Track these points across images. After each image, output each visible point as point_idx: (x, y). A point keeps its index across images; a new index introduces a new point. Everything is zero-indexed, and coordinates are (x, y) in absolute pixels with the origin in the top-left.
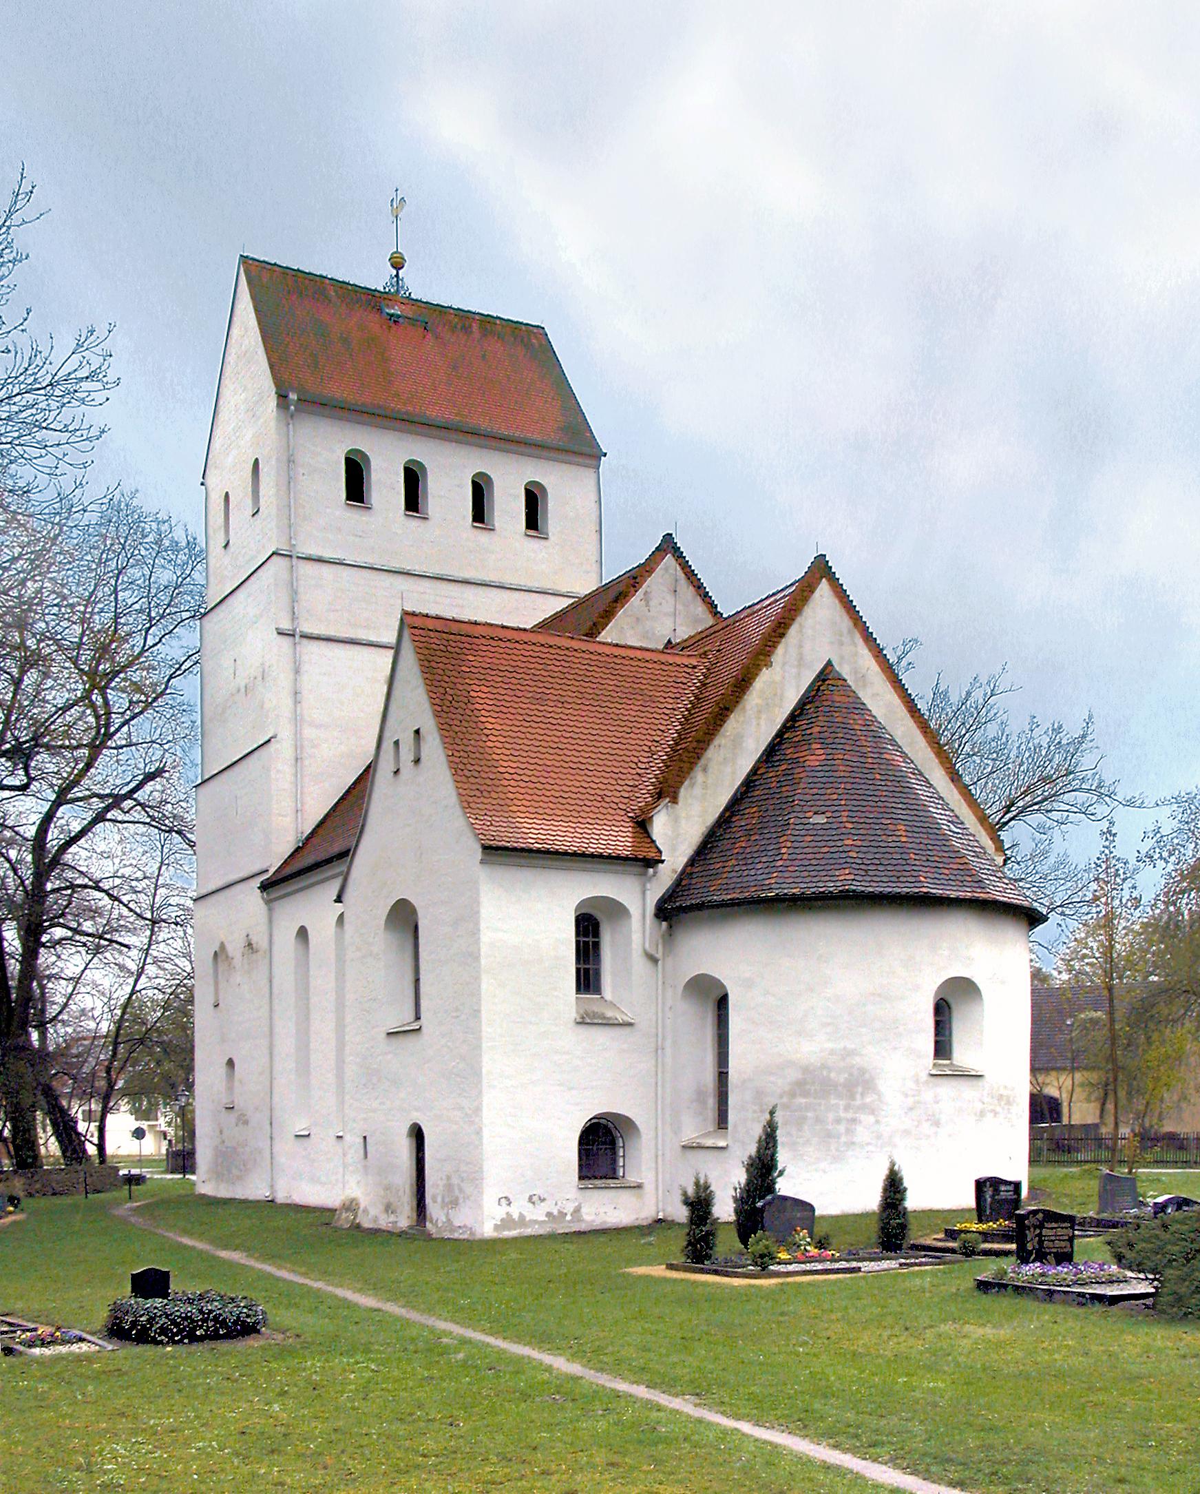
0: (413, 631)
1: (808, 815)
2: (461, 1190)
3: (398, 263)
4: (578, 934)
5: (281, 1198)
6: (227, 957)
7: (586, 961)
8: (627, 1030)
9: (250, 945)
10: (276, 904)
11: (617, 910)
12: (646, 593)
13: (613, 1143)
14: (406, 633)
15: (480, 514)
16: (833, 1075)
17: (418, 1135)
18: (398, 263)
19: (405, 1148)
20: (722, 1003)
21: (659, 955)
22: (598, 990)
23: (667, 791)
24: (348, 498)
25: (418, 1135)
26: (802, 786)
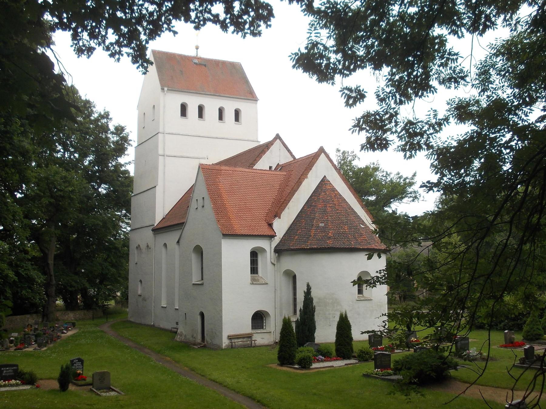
0: (203, 170)
1: (319, 223)
2: (216, 333)
3: (197, 48)
4: (251, 265)
5: (156, 325)
6: (141, 249)
7: (254, 265)
8: (267, 285)
9: (148, 246)
10: (156, 235)
11: (263, 250)
12: (271, 150)
13: (262, 318)
14: (201, 169)
15: (221, 118)
16: (327, 301)
17: (202, 315)
18: (197, 48)
19: (199, 318)
20: (294, 277)
21: (275, 263)
22: (257, 273)
23: (277, 215)
24: (181, 116)
25: (202, 315)
26: (317, 214)
